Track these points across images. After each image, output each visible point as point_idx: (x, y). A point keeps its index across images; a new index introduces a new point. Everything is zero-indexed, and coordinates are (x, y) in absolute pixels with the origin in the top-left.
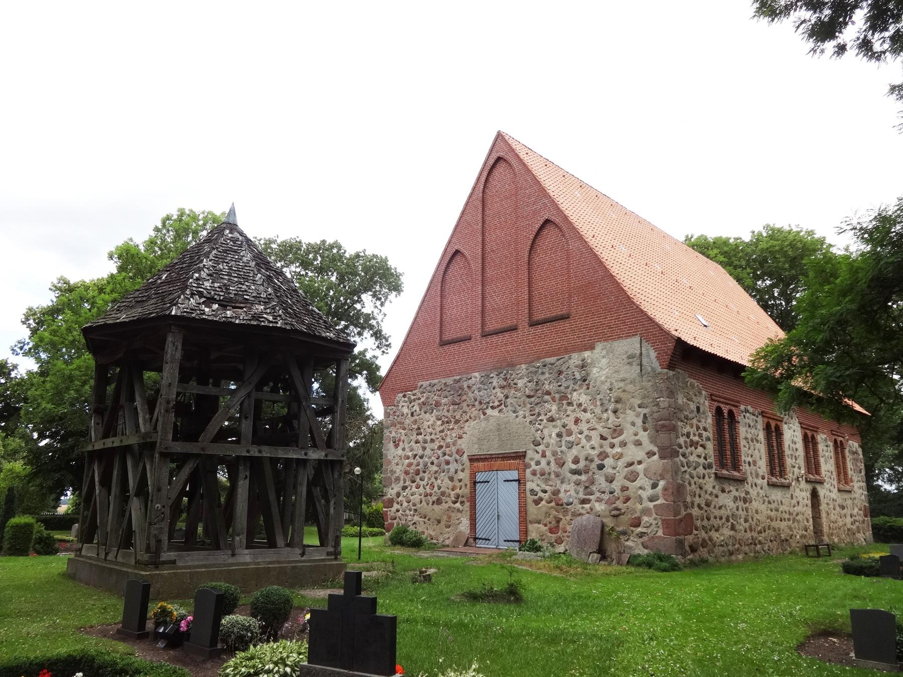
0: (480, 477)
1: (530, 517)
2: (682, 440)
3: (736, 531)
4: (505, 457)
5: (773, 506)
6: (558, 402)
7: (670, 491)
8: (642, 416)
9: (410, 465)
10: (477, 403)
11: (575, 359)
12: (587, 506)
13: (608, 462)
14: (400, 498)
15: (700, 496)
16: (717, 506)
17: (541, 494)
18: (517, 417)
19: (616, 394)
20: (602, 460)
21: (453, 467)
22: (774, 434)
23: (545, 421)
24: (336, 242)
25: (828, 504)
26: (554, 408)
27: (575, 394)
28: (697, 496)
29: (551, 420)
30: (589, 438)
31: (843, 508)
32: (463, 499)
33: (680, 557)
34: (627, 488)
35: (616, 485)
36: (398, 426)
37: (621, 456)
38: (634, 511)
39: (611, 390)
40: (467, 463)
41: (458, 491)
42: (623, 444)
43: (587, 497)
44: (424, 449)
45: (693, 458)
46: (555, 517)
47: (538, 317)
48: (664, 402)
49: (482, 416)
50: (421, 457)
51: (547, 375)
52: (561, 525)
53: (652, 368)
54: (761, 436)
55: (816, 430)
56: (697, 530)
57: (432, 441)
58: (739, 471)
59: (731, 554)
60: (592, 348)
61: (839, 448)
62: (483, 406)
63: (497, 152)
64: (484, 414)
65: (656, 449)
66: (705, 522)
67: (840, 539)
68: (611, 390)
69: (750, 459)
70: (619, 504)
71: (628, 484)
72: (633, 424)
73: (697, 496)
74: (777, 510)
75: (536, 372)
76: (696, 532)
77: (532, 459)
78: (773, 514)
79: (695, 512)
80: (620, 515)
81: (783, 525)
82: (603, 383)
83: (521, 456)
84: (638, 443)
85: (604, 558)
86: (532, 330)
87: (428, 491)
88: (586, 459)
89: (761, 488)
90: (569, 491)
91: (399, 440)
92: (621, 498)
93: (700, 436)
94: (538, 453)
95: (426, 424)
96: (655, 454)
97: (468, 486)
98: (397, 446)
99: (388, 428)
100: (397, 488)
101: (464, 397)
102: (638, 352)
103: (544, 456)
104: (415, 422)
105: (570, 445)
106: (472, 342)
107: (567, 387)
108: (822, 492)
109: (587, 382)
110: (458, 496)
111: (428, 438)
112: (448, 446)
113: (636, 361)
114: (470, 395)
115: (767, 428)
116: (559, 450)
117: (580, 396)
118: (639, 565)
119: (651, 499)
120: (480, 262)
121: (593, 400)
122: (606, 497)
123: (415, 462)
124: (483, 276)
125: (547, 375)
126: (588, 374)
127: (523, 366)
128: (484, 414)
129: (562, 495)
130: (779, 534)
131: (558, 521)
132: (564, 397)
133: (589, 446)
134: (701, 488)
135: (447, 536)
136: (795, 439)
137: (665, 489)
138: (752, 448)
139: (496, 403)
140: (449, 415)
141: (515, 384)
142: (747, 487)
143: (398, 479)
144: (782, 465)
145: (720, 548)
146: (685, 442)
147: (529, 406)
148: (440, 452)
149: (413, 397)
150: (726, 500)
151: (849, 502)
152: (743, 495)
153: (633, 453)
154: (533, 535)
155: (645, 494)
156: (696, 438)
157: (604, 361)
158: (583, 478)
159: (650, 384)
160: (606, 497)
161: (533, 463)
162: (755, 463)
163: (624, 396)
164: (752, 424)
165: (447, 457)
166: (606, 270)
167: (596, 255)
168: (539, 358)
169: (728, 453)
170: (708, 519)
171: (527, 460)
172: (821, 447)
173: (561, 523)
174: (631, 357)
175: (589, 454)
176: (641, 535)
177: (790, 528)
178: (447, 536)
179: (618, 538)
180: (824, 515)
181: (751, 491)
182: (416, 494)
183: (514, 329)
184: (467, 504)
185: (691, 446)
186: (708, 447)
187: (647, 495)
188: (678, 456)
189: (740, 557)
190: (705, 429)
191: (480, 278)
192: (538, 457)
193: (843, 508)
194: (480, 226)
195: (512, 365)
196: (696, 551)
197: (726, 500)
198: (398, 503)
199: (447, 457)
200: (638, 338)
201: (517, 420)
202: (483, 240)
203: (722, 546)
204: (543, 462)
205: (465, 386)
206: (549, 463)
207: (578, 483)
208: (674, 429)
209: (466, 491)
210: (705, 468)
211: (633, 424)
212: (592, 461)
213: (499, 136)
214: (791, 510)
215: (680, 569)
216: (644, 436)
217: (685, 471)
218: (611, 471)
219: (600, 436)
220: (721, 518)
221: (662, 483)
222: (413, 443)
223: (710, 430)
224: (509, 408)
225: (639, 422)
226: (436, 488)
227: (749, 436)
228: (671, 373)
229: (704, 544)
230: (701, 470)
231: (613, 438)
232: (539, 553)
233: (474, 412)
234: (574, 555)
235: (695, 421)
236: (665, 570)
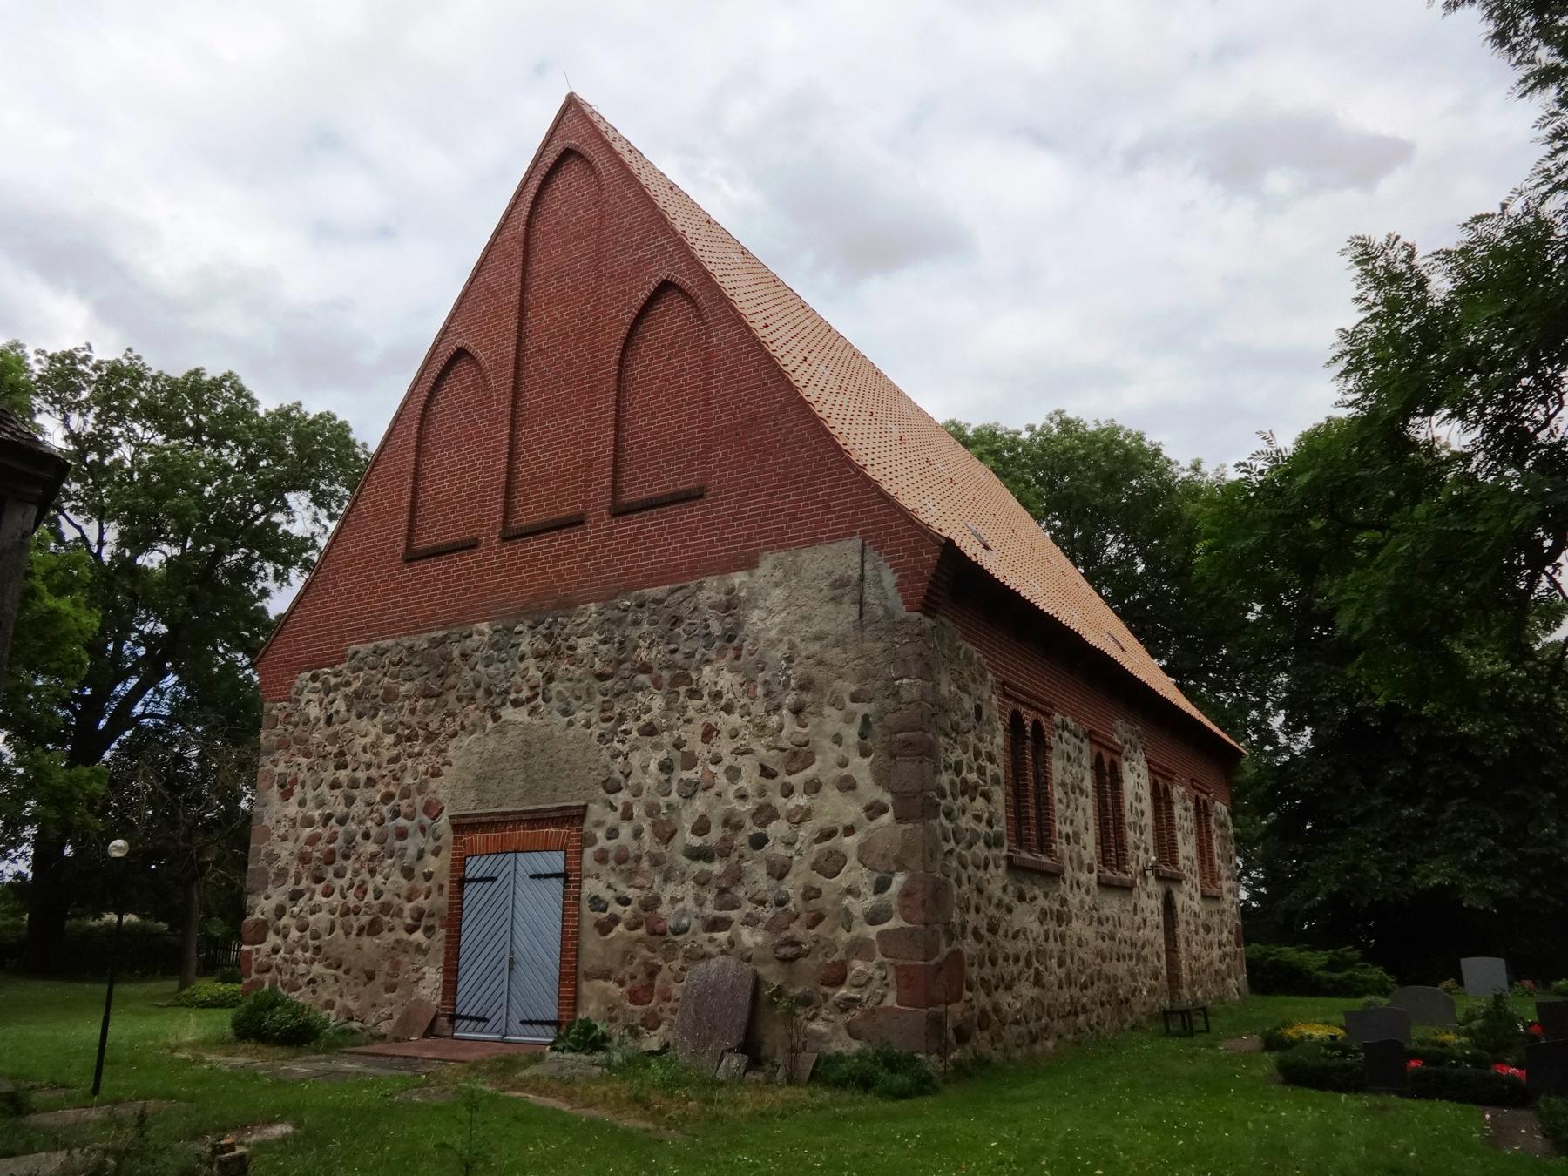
0: (474, 868)
1: (588, 962)
2: (945, 779)
3: (1043, 987)
4: (536, 819)
5: (1106, 928)
6: (666, 688)
7: (918, 896)
8: (858, 720)
9: (314, 840)
10: (480, 693)
11: (711, 590)
12: (722, 936)
13: (777, 829)
14: (285, 920)
15: (978, 910)
16: (1010, 934)
17: (615, 908)
18: (570, 724)
19: (800, 670)
20: (763, 825)
21: (412, 845)
22: (1107, 778)
23: (635, 734)
24: (228, 376)
25: (1188, 923)
26: (658, 702)
27: (707, 669)
28: (972, 909)
29: (650, 730)
30: (733, 773)
31: (1208, 929)
32: (431, 922)
33: (934, 1057)
34: (818, 892)
35: (792, 886)
36: (294, 748)
37: (805, 815)
38: (832, 946)
39: (789, 660)
40: (448, 835)
41: (421, 901)
42: (813, 787)
43: (723, 913)
44: (350, 801)
45: (965, 822)
46: (646, 963)
47: (632, 495)
48: (910, 687)
49: (490, 724)
50: (342, 821)
51: (646, 627)
52: (657, 983)
53: (886, 609)
54: (1088, 783)
55: (1169, 777)
56: (970, 989)
57: (371, 782)
58: (1049, 852)
59: (1034, 1039)
60: (750, 564)
61: (1202, 812)
62: (494, 698)
63: (564, 138)
64: (496, 718)
65: (887, 798)
66: (987, 971)
67: (1206, 992)
68: (789, 660)
69: (1067, 829)
70: (797, 930)
71: (820, 881)
72: (838, 739)
73: (972, 909)
74: (1112, 938)
75: (620, 620)
76: (967, 995)
77: (598, 824)
78: (1105, 945)
79: (969, 946)
80: (797, 956)
81: (1121, 968)
82: (773, 644)
83: (574, 816)
84: (847, 785)
85: (755, 1063)
86: (618, 525)
87: (352, 901)
88: (726, 823)
89: (1087, 892)
90: (680, 901)
91: (294, 782)
92: (803, 916)
93: (981, 771)
94: (614, 809)
95: (360, 741)
96: (884, 810)
97: (446, 889)
98: (286, 795)
99: (270, 753)
100: (278, 895)
101: (452, 680)
102: (856, 574)
103: (627, 815)
104: (334, 738)
105: (690, 791)
106: (480, 554)
107: (690, 655)
108: (1180, 899)
109: (736, 643)
110: (419, 914)
111: (361, 775)
112: (406, 794)
113: (850, 595)
114: (467, 674)
115: (1097, 766)
116: (663, 801)
117: (719, 677)
118: (841, 1084)
119: (873, 918)
120: (510, 372)
121: (748, 685)
122: (767, 913)
123: (326, 833)
124: (514, 405)
125: (646, 627)
126: (739, 625)
127: (593, 607)
128: (496, 718)
129: (664, 910)
130: (1116, 988)
131: (653, 971)
132: (681, 678)
133: (735, 793)
134: (980, 891)
135: (386, 1011)
136: (1141, 792)
137: (906, 893)
138: (1072, 805)
139: (525, 693)
140: (414, 721)
141: (571, 648)
142: (1064, 888)
143: (282, 875)
144: (1121, 843)
145: (1014, 1028)
146: (952, 783)
147: (599, 698)
148: (385, 809)
149: (333, 681)
150: (1027, 919)
151: (1216, 918)
152: (1056, 906)
153: (836, 808)
154: (590, 1010)
155: (858, 907)
156: (973, 777)
157: (778, 594)
158: (717, 867)
159: (880, 645)
160: (767, 913)
161: (600, 834)
162: (1077, 834)
163: (819, 674)
164: (1073, 755)
165: (401, 821)
166: (791, 389)
167: (769, 358)
168: (629, 589)
169: (1032, 813)
170: (993, 963)
171: (587, 826)
172: (1178, 810)
173: (659, 977)
174: (840, 583)
175: (732, 812)
176: (847, 1005)
177: (1133, 975)
178: (384, 1017)
179: (791, 1013)
180: (1182, 945)
181: (1070, 897)
182: (320, 907)
183: (576, 522)
184: (441, 933)
185: (963, 794)
186: (995, 797)
187: (863, 903)
188: (937, 816)
189: (1050, 1044)
190: (991, 759)
191: (508, 410)
192: (612, 818)
193: (1208, 929)
194: (515, 297)
195: (568, 605)
196: (967, 1040)
197: (1025, 918)
198: (277, 932)
199: (401, 821)
200: (855, 542)
201: (571, 732)
202: (521, 326)
203: (1017, 1022)
204: (626, 830)
205: (456, 653)
206: (637, 834)
207: (703, 881)
208: (930, 751)
209: (441, 901)
210: (988, 845)
211: (838, 739)
212: (739, 827)
213: (572, 106)
214: (1135, 937)
215: (935, 1090)
216: (861, 768)
217: (951, 852)
218: (781, 850)
219: (756, 771)
220: (1017, 960)
221: (899, 880)
222: (324, 788)
223: (1000, 760)
224: (555, 703)
225: (852, 734)
226: (370, 896)
227: (1069, 780)
228: (928, 623)
229: (983, 1022)
230: (980, 849)
231: (790, 773)
232: (600, 1056)
233: (473, 713)
234: (684, 1057)
235: (971, 737)
236: (902, 1095)
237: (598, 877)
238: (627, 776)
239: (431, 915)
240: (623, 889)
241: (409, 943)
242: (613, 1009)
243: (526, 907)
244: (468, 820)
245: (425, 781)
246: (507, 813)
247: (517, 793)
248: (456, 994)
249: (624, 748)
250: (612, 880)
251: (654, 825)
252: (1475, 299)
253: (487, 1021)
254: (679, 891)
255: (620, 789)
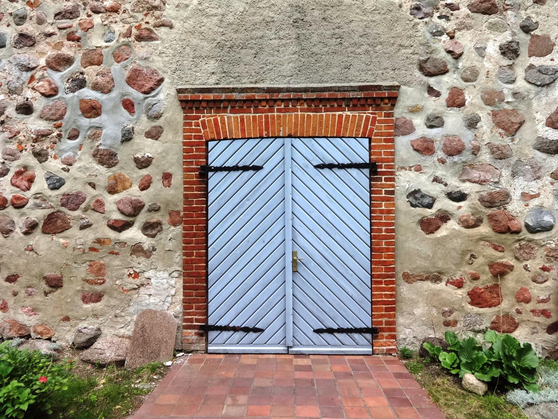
0: (219, 154)
32: (155, 217)
40: (174, 114)
77: (415, 110)
83: (380, 99)
97: (178, 178)
103: (456, 101)
112: (94, 59)
116: (507, 89)
129: (515, 206)
148: (56, 77)
161: (418, 121)
165: (88, 93)
171: (399, 112)
199: (88, 93)
204: (454, 121)
209: (175, 194)
237: (418, 169)
238: (457, 57)
239: (155, 209)
240: (455, 184)
241: (123, 244)
242: (451, 312)
243: (296, 210)
244: (211, 96)
245: (127, 45)
246: (279, 90)
247: (287, 68)
248: (206, 301)
249: (449, 26)
250: (440, 172)
251: (494, 115)
252: (387, 167)
253: (261, 331)
254: (533, 187)
255: (444, 72)
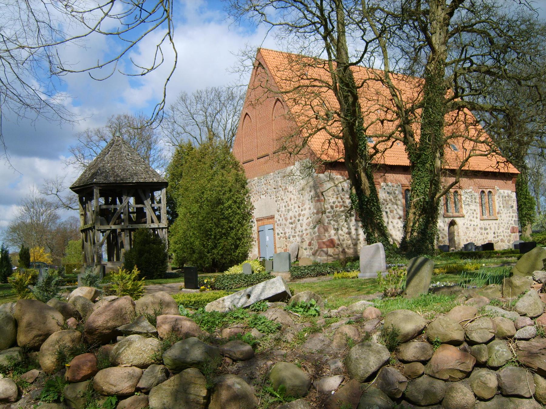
158: (294, 226)
161: (277, 221)
184: (257, 241)
